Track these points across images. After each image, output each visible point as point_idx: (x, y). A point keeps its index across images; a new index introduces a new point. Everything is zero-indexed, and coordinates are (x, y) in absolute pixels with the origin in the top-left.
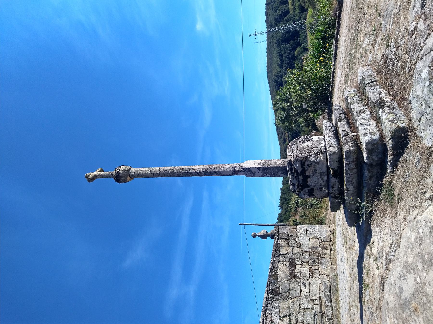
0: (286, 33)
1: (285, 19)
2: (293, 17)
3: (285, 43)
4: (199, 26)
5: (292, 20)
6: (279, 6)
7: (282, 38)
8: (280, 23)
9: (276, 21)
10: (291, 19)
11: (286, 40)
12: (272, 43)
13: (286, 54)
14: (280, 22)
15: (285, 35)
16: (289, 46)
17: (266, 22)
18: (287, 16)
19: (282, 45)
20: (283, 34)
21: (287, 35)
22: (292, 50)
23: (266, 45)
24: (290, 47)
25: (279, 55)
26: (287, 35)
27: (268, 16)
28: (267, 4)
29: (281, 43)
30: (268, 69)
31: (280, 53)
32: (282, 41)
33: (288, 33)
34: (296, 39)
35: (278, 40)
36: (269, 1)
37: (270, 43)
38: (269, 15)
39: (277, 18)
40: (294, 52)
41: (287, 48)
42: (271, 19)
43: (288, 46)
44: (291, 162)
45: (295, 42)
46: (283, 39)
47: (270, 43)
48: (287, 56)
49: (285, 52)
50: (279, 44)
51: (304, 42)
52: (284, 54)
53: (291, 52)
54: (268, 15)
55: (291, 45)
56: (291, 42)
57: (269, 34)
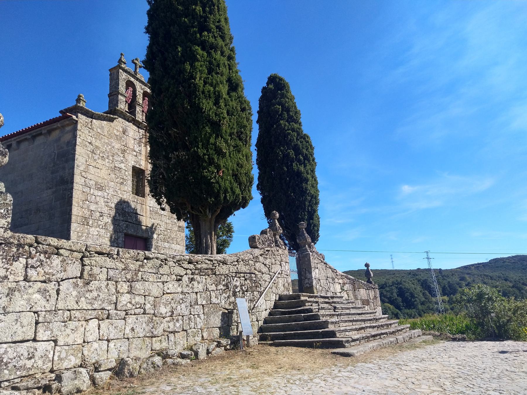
0: (410, 293)
1: (425, 292)
2: (428, 301)
3: (398, 292)
4: (406, 189)
5: (425, 301)
6: (440, 285)
7: (405, 288)
8: (421, 285)
9: (423, 281)
10: (426, 298)
11: (401, 292)
12: (395, 276)
13: (385, 293)
14: (422, 285)
15: (407, 292)
16: (395, 296)
17: (419, 269)
18: (429, 295)
19: (396, 288)
20: (408, 290)
21: (408, 294)
22: (390, 301)
23: (390, 269)
24: (394, 298)
25: (383, 285)
26: (408, 294)
27: (426, 272)
28: (440, 271)
29: (397, 287)
30: (515, 259)
31: (386, 285)
32: (401, 288)
33: (410, 296)
34: (403, 305)
35: (401, 284)
36: (443, 273)
37: (394, 274)
38: (427, 272)
39: (426, 282)
40: (388, 303)
41: (392, 294)
42: (423, 276)
43: (395, 295)
44: (73, 114)
45: (400, 304)
46: (403, 289)
47: (394, 274)
48: (383, 294)
49: (387, 291)
50: (396, 284)
51: (404, 314)
52: (386, 290)
53: (388, 298)
54: (427, 271)
55: (396, 299)
56: (400, 299)
57: (429, 270)
